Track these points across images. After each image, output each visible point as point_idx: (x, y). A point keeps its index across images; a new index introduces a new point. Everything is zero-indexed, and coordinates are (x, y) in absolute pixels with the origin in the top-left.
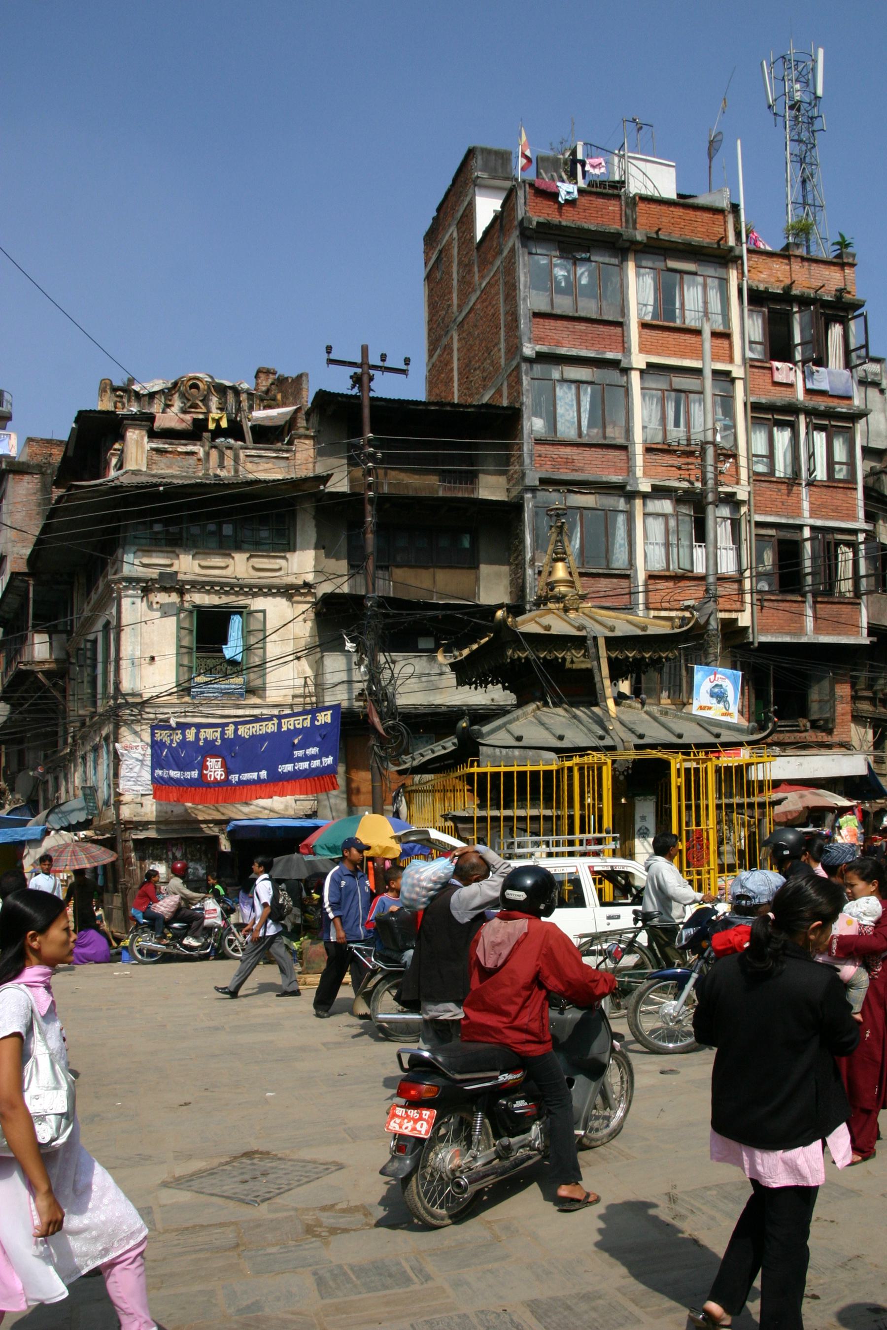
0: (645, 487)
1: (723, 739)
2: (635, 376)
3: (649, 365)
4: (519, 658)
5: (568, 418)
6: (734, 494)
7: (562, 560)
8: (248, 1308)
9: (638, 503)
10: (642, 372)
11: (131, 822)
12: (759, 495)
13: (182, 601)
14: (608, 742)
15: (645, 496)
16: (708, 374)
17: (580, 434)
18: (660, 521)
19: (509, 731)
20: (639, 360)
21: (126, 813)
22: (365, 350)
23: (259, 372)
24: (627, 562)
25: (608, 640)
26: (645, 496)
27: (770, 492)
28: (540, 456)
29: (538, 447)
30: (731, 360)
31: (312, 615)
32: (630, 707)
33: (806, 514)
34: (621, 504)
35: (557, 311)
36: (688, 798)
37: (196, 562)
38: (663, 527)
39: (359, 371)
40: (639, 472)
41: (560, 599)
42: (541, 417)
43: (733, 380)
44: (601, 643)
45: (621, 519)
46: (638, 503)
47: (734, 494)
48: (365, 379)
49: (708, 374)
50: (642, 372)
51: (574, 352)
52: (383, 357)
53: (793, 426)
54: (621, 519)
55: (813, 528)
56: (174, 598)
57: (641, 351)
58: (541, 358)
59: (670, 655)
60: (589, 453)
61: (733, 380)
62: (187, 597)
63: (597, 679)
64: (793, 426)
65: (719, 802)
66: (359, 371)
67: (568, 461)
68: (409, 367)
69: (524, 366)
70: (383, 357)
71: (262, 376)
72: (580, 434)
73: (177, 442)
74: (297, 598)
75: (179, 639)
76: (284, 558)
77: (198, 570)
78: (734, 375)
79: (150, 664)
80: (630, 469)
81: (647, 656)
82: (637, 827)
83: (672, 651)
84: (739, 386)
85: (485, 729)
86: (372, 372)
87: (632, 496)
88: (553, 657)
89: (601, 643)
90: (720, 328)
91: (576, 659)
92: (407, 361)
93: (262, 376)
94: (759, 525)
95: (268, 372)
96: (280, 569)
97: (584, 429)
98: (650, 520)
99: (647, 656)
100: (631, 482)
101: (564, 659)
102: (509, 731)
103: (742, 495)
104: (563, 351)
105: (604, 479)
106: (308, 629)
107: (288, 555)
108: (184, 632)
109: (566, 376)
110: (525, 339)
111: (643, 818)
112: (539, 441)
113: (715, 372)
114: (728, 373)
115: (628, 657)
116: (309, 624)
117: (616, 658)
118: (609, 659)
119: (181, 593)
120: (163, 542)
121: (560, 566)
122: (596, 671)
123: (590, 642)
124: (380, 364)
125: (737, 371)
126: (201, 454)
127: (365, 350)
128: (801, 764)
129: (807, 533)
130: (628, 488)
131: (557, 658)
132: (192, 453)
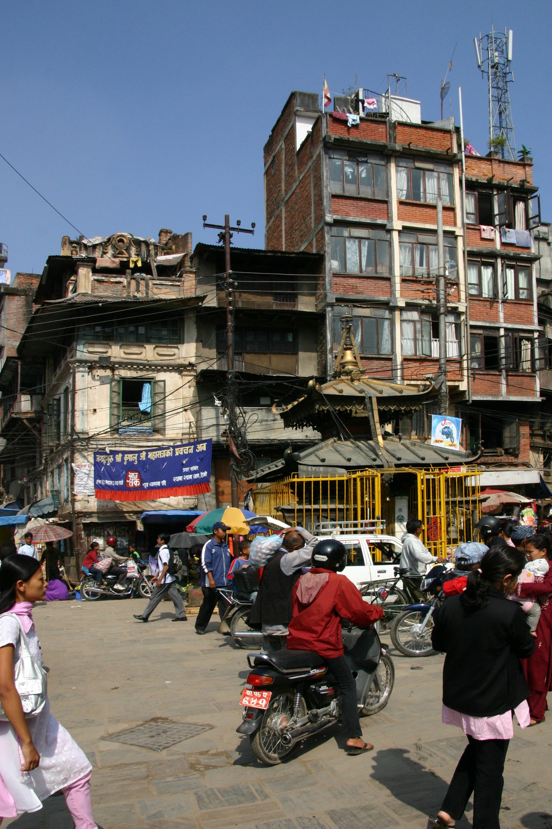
0: (401, 303)
1: (450, 461)
2: (395, 235)
3: (404, 227)
4: (323, 410)
5: (353, 260)
6: (457, 308)
7: (350, 349)
8: (154, 815)
9: (397, 313)
10: (399, 232)
11: (81, 512)
12: (472, 308)
13: (113, 375)
14: (378, 462)
15: (401, 309)
16: (441, 233)
17: (361, 271)
18: (411, 325)
19: (316, 456)
20: (397, 225)
21: (78, 507)
22: (227, 218)
23: (161, 232)
24: (390, 350)
25: (378, 399)
26: (401, 309)
27: (479, 307)
28: (336, 284)
29: (335, 279)
30: (455, 225)
31: (194, 384)
32: (392, 440)
33: (502, 320)
34: (387, 314)
35: (347, 194)
36: (428, 497)
37: (122, 350)
38: (412, 328)
39: (223, 231)
40: (398, 294)
41: (348, 373)
42: (337, 260)
43: (456, 237)
44: (374, 400)
45: (386, 323)
46: (397, 313)
47: (457, 308)
48: (227, 236)
49: (441, 233)
50: (399, 232)
51: (357, 219)
52: (239, 223)
53: (493, 266)
54: (386, 323)
55: (506, 329)
56: (108, 373)
57: (399, 219)
58: (337, 223)
59: (417, 408)
60: (366, 282)
61: (456, 237)
62: (116, 372)
63: (372, 423)
64: (493, 266)
66: (223, 231)
67: (354, 288)
68: (255, 229)
69: (326, 228)
70: (239, 223)
71: (163, 234)
72: (361, 271)
73: (110, 275)
74: (185, 373)
75: (111, 398)
76: (177, 348)
77: (123, 355)
78: (457, 234)
79: (93, 414)
80: (392, 293)
81: (403, 409)
82: (396, 516)
83: (418, 406)
84: (460, 240)
85: (302, 454)
86: (231, 232)
87: (393, 309)
88: (344, 409)
89: (374, 400)
90: (448, 205)
91: (358, 411)
92: (253, 225)
93: (163, 234)
94: (472, 327)
95: (167, 232)
96: (174, 355)
97: (364, 268)
98: (405, 324)
99: (403, 409)
100: (393, 300)
101: (351, 411)
102: (316, 456)
103: (462, 309)
104: (350, 219)
105: (376, 299)
106: (192, 392)
107: (179, 346)
108: (114, 394)
109: (352, 234)
110: (327, 211)
111: (400, 510)
112: (335, 275)
113: (445, 232)
114: (453, 233)
115: (391, 410)
116: (192, 389)
117: (384, 410)
118: (379, 411)
119: (113, 369)
120: (102, 338)
121: (348, 353)
122: (371, 418)
123: (367, 400)
124: (237, 227)
125: (459, 231)
126: (125, 283)
127: (227, 218)
129: (502, 332)
130: (391, 304)
131: (346, 410)
132: (120, 283)
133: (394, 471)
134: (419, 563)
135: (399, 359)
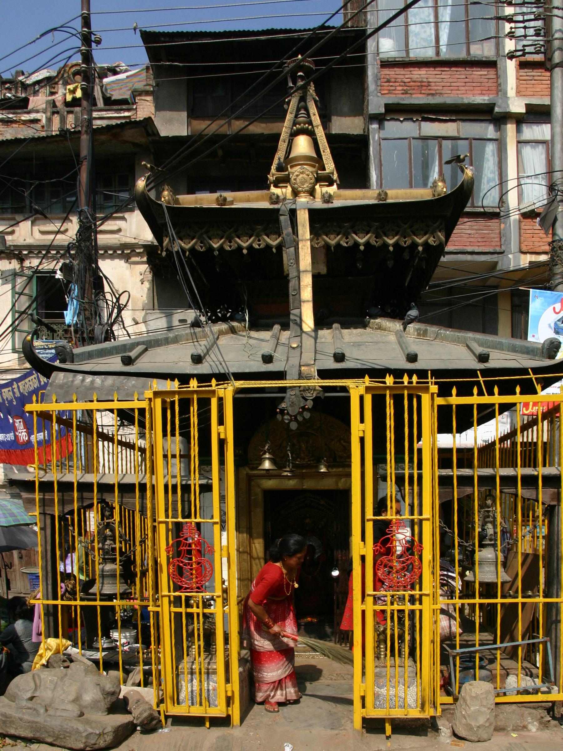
0: (517, 106)
5: (423, 36)
8: (456, 745)
9: (511, 128)
13: (22, 267)
15: (520, 120)
17: (438, 53)
18: (540, 151)
24: (497, 200)
28: (388, 81)
29: (386, 71)
31: (150, 276)
32: (380, 328)
34: (490, 131)
37: (36, 229)
38: (543, 157)
40: (511, 91)
42: (390, 38)
44: (303, 217)
45: (490, 149)
46: (511, 128)
54: (490, 149)
56: (14, 265)
59: (431, 241)
60: (447, 74)
62: (27, 263)
65: (445, 472)
67: (423, 85)
72: (438, 53)
73: (19, 111)
74: (134, 259)
76: (123, 218)
77: (37, 235)
80: (499, 87)
81: (391, 242)
83: (433, 233)
87: (500, 119)
88: (234, 246)
89: (303, 217)
96: (119, 230)
97: (443, 49)
98: (527, 150)
99: (391, 242)
100: (499, 102)
105: (466, 101)
106: (146, 290)
107: (127, 215)
112: (386, 64)
115: (356, 244)
116: (147, 285)
117: (338, 245)
119: (21, 260)
120: (9, 210)
123: (284, 219)
126: (44, 121)
128: (25, 240)
130: (497, 109)
132: (36, 121)
133: (317, 383)
134: (242, 656)
135: (515, 217)
